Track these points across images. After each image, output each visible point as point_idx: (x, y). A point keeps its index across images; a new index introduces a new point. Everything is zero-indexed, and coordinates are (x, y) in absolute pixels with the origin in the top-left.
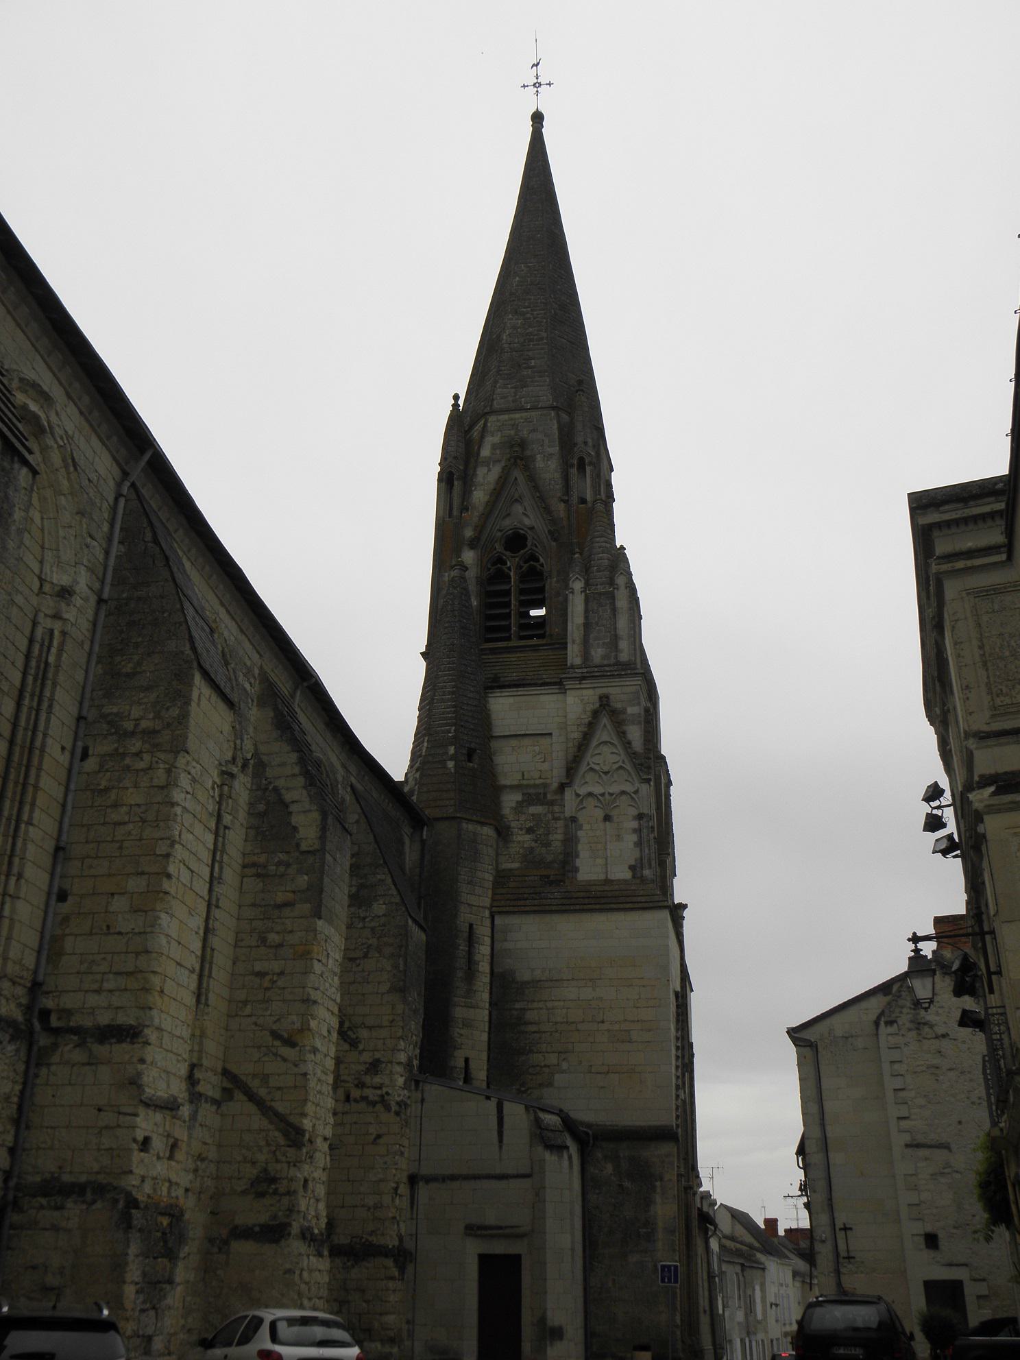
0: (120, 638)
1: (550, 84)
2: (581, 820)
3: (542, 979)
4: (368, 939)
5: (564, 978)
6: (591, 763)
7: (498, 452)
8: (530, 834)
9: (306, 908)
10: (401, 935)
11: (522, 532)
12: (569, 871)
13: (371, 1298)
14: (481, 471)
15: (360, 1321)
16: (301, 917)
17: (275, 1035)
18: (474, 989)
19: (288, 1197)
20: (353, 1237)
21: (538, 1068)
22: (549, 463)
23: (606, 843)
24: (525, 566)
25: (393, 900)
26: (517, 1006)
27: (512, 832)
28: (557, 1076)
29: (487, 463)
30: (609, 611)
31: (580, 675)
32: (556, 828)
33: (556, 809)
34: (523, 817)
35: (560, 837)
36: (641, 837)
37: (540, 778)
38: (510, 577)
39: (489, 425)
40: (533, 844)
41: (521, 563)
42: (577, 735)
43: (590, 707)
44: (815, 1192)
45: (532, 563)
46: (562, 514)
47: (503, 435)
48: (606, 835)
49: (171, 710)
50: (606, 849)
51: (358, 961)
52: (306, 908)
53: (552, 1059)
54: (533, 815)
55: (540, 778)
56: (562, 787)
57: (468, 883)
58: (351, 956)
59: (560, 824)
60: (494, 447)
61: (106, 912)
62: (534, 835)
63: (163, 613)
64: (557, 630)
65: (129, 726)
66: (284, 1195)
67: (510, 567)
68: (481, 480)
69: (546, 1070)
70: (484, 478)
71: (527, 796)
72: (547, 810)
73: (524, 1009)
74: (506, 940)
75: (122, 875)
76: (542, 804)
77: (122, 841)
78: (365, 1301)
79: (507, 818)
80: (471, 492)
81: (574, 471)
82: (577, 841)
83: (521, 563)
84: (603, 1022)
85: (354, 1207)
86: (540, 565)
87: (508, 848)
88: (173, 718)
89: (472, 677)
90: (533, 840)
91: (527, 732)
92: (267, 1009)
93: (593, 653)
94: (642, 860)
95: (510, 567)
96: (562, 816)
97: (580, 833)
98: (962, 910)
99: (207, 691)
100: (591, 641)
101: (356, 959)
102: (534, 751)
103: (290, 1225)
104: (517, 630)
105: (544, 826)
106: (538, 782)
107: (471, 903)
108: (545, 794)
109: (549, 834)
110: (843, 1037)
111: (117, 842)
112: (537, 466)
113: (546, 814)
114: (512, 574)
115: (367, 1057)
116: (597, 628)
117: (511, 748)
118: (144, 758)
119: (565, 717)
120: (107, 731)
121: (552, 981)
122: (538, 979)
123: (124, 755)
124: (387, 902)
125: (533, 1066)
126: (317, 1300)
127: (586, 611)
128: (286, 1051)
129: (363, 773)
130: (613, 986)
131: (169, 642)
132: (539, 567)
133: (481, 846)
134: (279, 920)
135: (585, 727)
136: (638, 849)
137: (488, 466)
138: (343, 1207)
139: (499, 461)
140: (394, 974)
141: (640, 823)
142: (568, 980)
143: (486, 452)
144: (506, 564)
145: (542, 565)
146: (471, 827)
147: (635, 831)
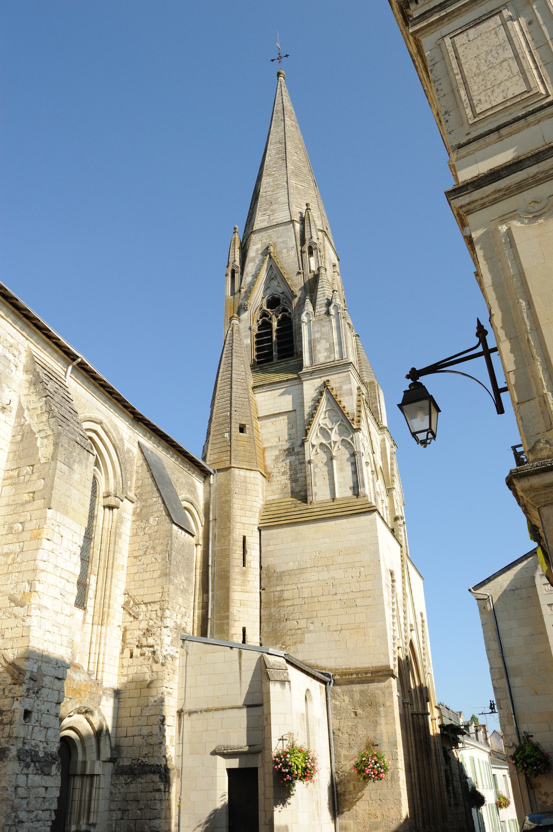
4: (147, 542)
9: (40, 503)
10: (167, 536)
11: (277, 296)
13: (143, 807)
15: (135, 826)
17: (12, 599)
19: (9, 726)
20: (133, 760)
21: (294, 631)
26: (278, 588)
28: (306, 635)
44: (501, 708)
51: (140, 558)
53: (303, 624)
58: (136, 555)
66: (7, 724)
69: (299, 632)
73: (282, 590)
78: (140, 810)
81: (306, 255)
84: (336, 594)
85: (133, 736)
89: (242, 381)
92: (8, 579)
98: (489, 348)
101: (139, 556)
103: (8, 749)
107: (244, 522)
110: (511, 590)
115: (144, 625)
125: (291, 630)
126: (40, 812)
128: (18, 610)
134: (23, 514)
138: (126, 737)
145: (290, 313)
146: (242, 472)
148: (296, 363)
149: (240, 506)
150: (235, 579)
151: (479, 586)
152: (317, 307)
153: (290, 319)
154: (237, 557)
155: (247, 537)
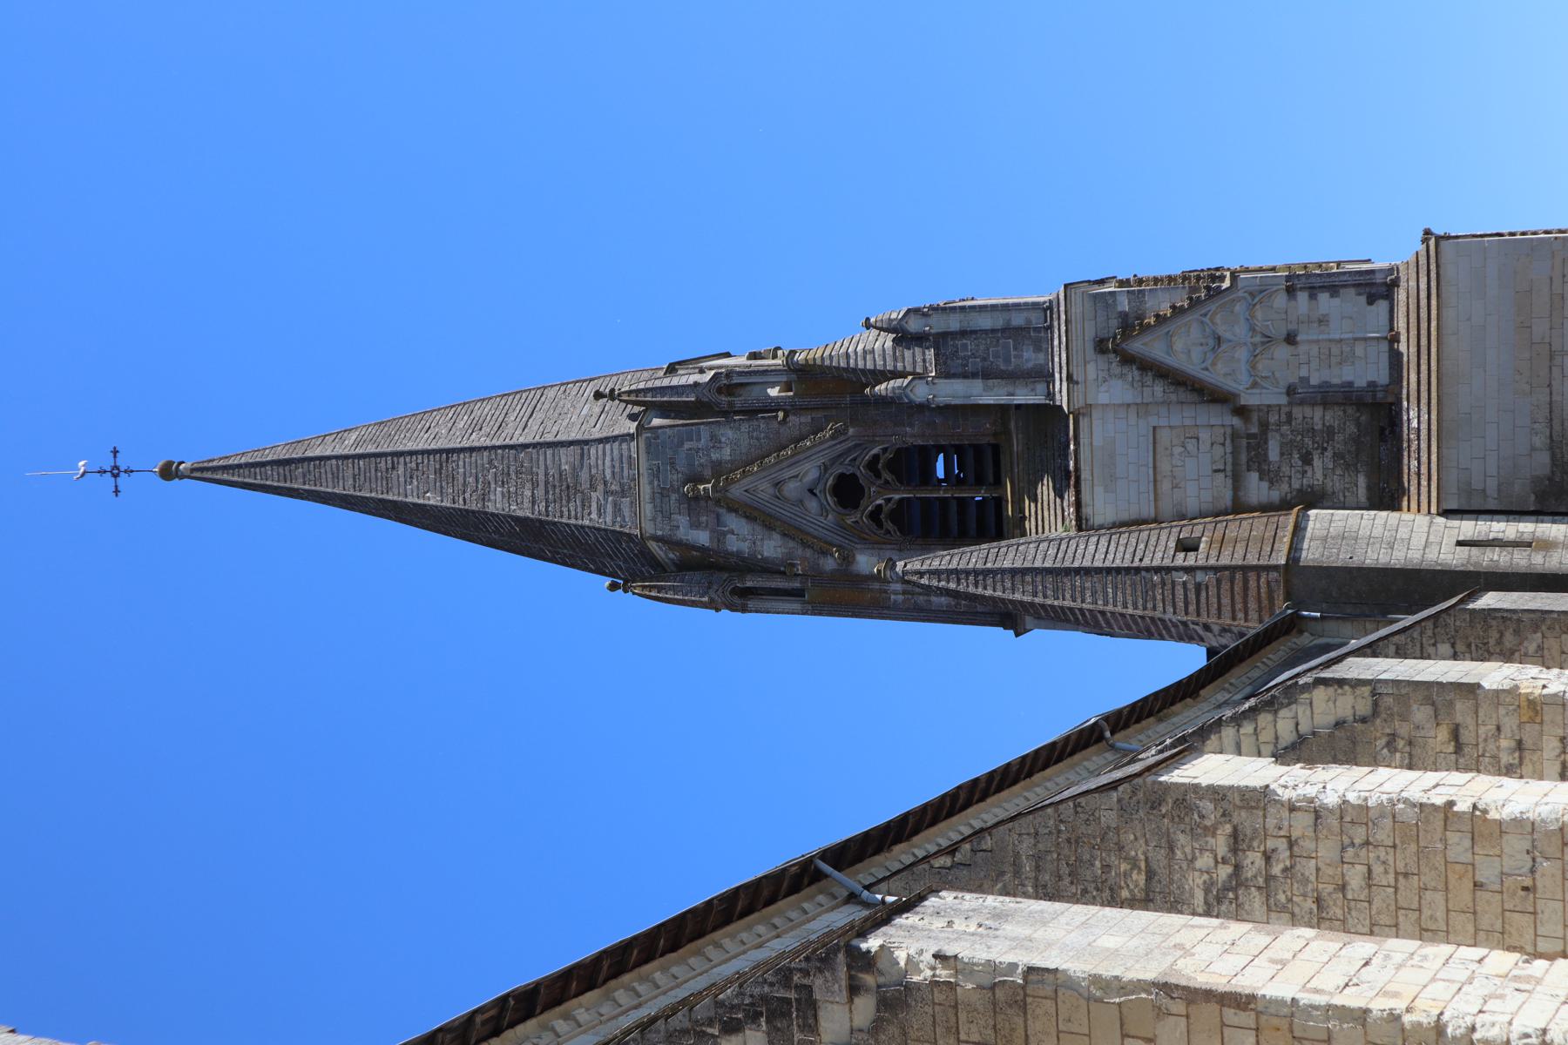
0: (1095, 893)
1: (115, 452)
2: (1293, 379)
3: (1548, 434)
5: (1548, 399)
6: (1203, 365)
7: (704, 519)
8: (1312, 459)
12: (1374, 396)
14: (733, 544)
16: (1476, 713)
18: (1563, 538)
22: (723, 439)
23: (1330, 340)
24: (887, 475)
25: (1429, 633)
27: (1309, 486)
29: (720, 536)
30: (965, 341)
31: (1065, 384)
32: (1304, 418)
33: (1273, 418)
34: (1285, 469)
35: (1318, 412)
36: (1320, 287)
37: (1223, 444)
38: (902, 500)
39: (660, 533)
40: (1329, 454)
41: (881, 482)
42: (1159, 388)
43: (1116, 369)
45: (880, 466)
46: (806, 419)
47: (678, 511)
48: (1318, 341)
49: (1204, 812)
50: (1341, 340)
52: (1462, 708)
54: (1282, 454)
55: (1223, 444)
56: (1242, 411)
57: (1392, 548)
59: (1297, 412)
60: (695, 525)
61: (1502, 892)
62: (1314, 453)
63: (1059, 831)
64: (988, 426)
65: (1224, 871)
67: (885, 499)
68: (747, 544)
70: (744, 540)
71: (1251, 463)
72: (1274, 433)
74: (1484, 491)
75: (1446, 871)
76: (1266, 442)
77: (1396, 873)
79: (1286, 493)
80: (765, 560)
82: (1326, 384)
83: (881, 482)
86: (884, 453)
87: (1334, 493)
88: (1215, 808)
90: (1323, 454)
91: (1151, 465)
93: (1030, 365)
94: (1359, 285)
95: (885, 499)
96: (1285, 410)
97: (1314, 381)
99: (1169, 770)
100: (1010, 368)
102: (1180, 454)
104: (984, 487)
105: (1300, 437)
106: (1229, 449)
107: (1423, 543)
108: (1249, 436)
109: (1313, 429)
111: (1396, 880)
112: (728, 458)
113: (1282, 435)
114: (897, 497)
116: (991, 359)
117: (1175, 490)
118: (1273, 847)
119: (1129, 405)
120: (1231, 903)
121: (1551, 419)
122: (1548, 441)
123: (1269, 878)
124: (1433, 641)
127: (965, 376)
129: (1227, 685)
130: (1563, 324)
131: (1103, 819)
132: (887, 455)
133: (1331, 529)
135: (1147, 375)
136: (1342, 291)
137: (724, 534)
139: (718, 516)
140: (1549, 629)
141: (1301, 289)
142: (1551, 394)
143: (702, 538)
144: (880, 505)
145: (885, 450)
147: (1313, 297)
148: (1020, 436)
149: (1383, 550)
150: (1561, 563)
151: (1477, 543)
152: (900, 366)
153: (899, 451)
154: (1508, 558)
155: (1461, 538)
